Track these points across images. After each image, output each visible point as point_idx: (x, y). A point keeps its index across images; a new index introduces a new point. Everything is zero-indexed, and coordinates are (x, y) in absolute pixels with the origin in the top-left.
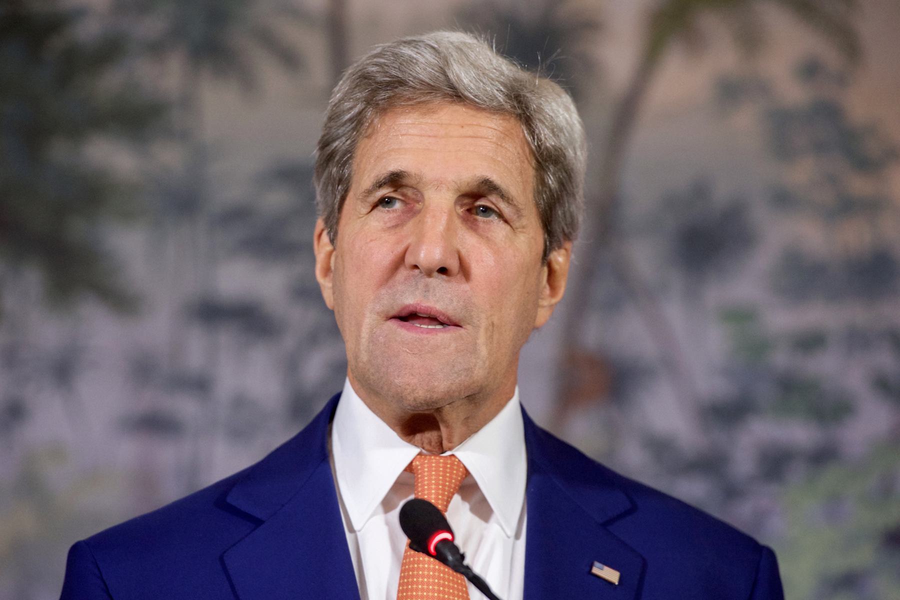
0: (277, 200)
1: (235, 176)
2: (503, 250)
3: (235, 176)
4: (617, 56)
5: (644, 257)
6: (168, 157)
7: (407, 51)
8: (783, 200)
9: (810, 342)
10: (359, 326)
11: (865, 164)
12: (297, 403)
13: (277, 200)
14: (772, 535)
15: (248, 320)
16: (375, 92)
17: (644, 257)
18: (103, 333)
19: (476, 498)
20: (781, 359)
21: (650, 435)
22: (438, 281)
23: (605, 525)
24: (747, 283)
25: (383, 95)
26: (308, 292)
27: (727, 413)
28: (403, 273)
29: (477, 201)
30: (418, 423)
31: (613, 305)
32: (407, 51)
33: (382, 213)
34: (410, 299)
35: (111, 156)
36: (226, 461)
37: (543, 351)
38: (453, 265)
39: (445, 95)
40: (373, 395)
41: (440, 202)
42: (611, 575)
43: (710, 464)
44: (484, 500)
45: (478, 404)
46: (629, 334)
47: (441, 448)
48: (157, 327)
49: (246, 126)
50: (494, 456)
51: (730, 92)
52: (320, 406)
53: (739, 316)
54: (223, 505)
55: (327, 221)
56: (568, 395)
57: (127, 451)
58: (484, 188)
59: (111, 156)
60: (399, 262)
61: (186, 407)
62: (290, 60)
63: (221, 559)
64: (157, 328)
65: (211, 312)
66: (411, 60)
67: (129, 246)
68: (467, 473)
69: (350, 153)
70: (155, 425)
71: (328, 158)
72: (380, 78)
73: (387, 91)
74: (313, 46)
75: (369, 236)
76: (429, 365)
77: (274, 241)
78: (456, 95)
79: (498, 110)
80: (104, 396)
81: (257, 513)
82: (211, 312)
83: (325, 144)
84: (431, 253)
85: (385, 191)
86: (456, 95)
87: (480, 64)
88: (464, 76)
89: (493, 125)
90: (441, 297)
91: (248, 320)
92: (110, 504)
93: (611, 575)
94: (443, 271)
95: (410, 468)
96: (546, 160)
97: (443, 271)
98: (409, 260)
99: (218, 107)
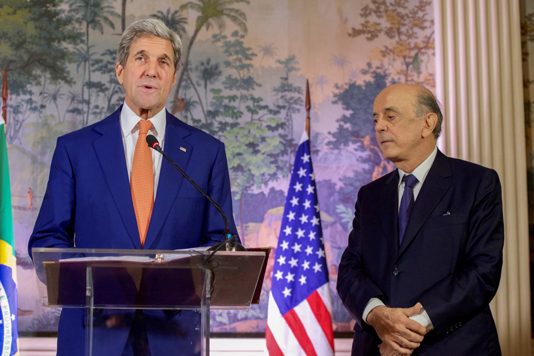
0: (107, 58)
1: (97, 53)
2: (167, 72)
3: (97, 53)
4: (190, 28)
5: (194, 76)
6: (82, 47)
7: (145, 23)
8: (228, 64)
9: (233, 98)
10: (132, 88)
11: (247, 57)
12: (109, 108)
13: (107, 58)
14: (222, 140)
15: (99, 87)
16: (137, 33)
17: (194, 76)
18: (64, 88)
19: (154, 131)
20: (226, 102)
21: (195, 116)
22: (152, 79)
23: (183, 138)
24: (218, 84)
25: (139, 34)
26: (114, 81)
27: (213, 114)
28: (143, 77)
29: (162, 60)
30: (144, 112)
31: (186, 87)
32: (145, 23)
33: (138, 61)
34: (146, 83)
35: (67, 46)
36: (92, 120)
37: (171, 98)
38: (156, 75)
39: (155, 35)
40: (133, 105)
41: (153, 59)
42: (184, 150)
43: (209, 126)
44: (156, 131)
45: (159, 107)
46: (190, 95)
47: (146, 119)
48: (77, 88)
49: (101, 40)
50: (159, 122)
51: (216, 38)
52: (117, 108)
53: (216, 91)
54: (93, 131)
55: (121, 63)
56: (175, 108)
57: (69, 117)
58: (164, 57)
59: (67, 46)
60: (143, 74)
61: (85, 108)
62: (112, 25)
63: (92, 143)
64: (77, 88)
65: (90, 85)
66: (146, 26)
67: (71, 67)
68: (152, 125)
69: (128, 48)
70: (76, 111)
71: (122, 48)
72: (137, 29)
73: (139, 32)
74: (118, 23)
75: (135, 67)
76: (148, 100)
77: (106, 69)
78: (158, 35)
79: (167, 39)
80: (64, 104)
81: (102, 132)
82: (90, 85)
83: (121, 44)
84: (152, 72)
85: (139, 56)
86: (158, 35)
87: (161, 27)
88: (160, 31)
89: (163, 43)
90: (153, 83)
91: (99, 87)
92: (66, 130)
93: (184, 150)
94: (154, 77)
95: (139, 123)
96: (176, 51)
97: (154, 77)
98: (146, 74)
99: (94, 35)
